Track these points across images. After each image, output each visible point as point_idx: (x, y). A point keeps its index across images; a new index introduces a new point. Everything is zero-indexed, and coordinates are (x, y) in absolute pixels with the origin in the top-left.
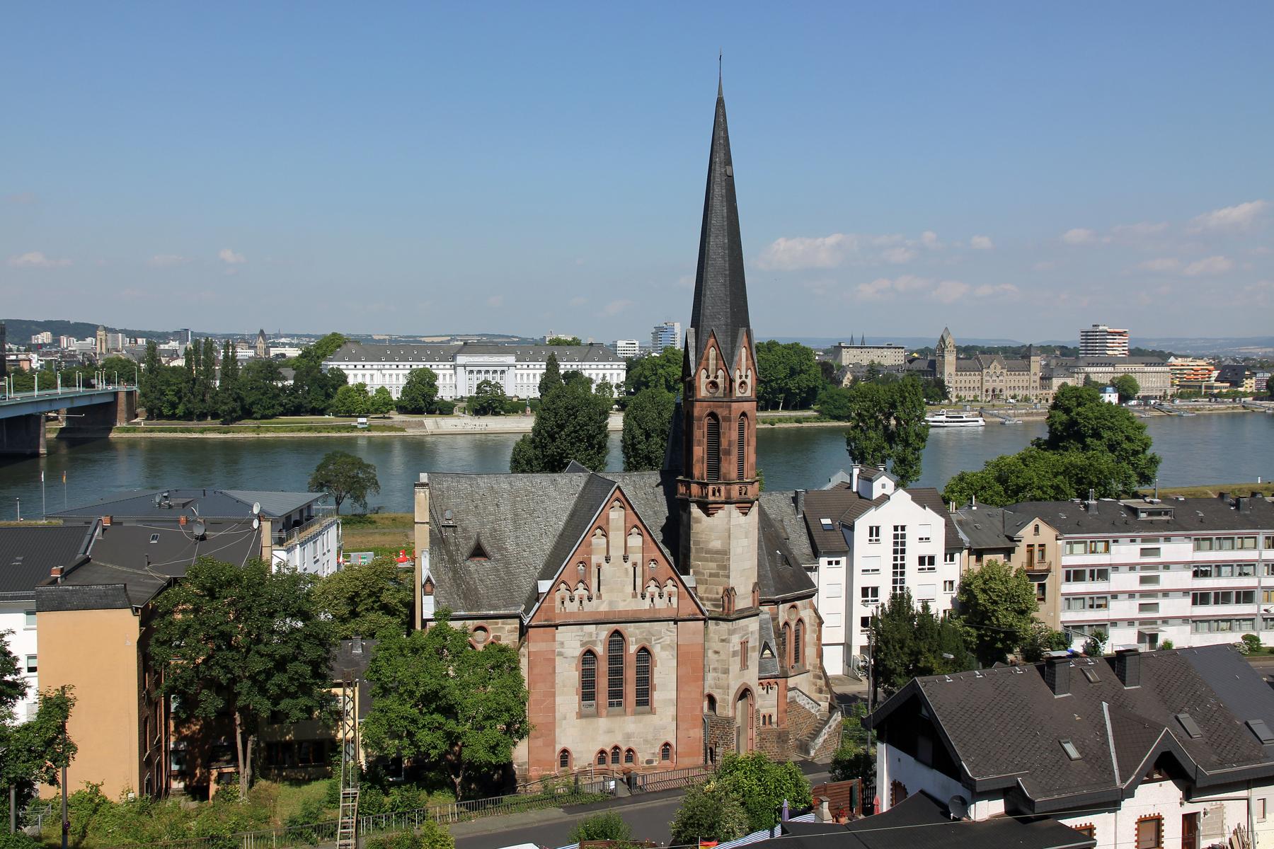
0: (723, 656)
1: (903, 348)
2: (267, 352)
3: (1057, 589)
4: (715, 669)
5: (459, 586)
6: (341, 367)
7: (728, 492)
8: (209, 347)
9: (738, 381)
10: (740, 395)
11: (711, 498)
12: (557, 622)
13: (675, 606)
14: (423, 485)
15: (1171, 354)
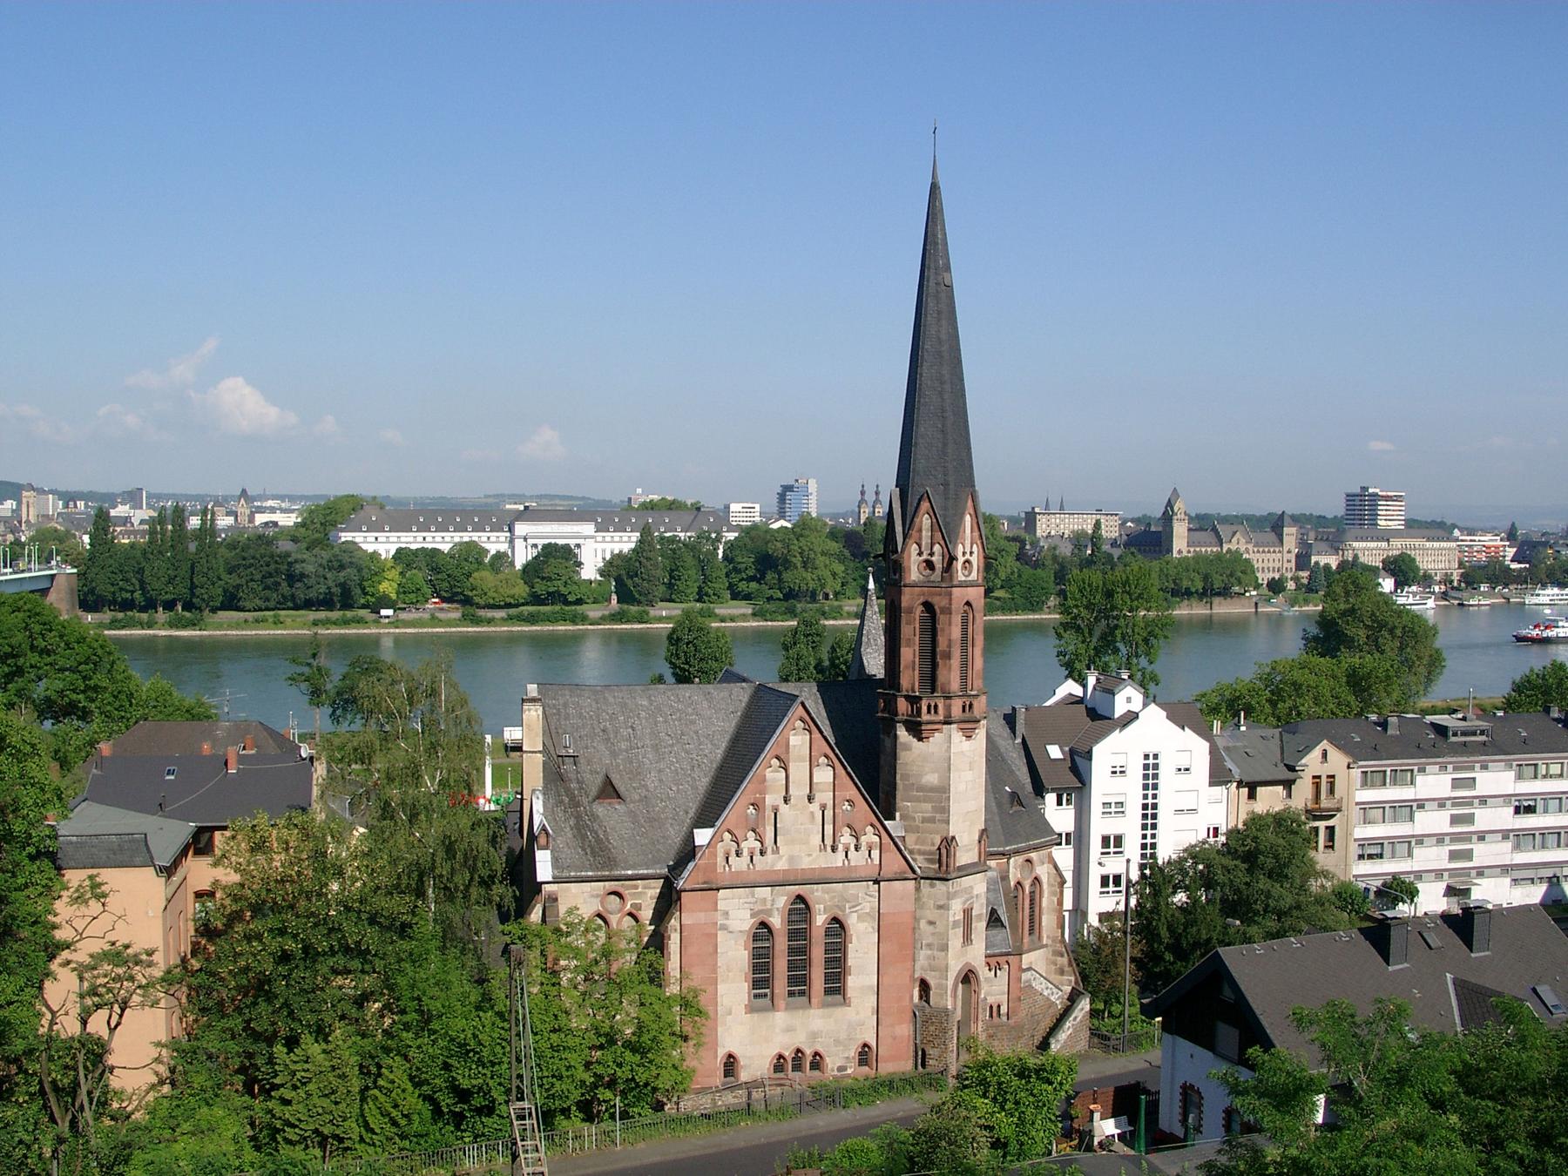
0: (940, 928)
1: (1116, 515)
2: (251, 520)
3: (1348, 833)
4: (929, 946)
5: (584, 837)
6: (357, 540)
7: (948, 708)
8: (179, 515)
9: (961, 560)
10: (963, 579)
11: (925, 717)
12: (719, 886)
13: (877, 862)
14: (533, 700)
15: (1454, 526)
